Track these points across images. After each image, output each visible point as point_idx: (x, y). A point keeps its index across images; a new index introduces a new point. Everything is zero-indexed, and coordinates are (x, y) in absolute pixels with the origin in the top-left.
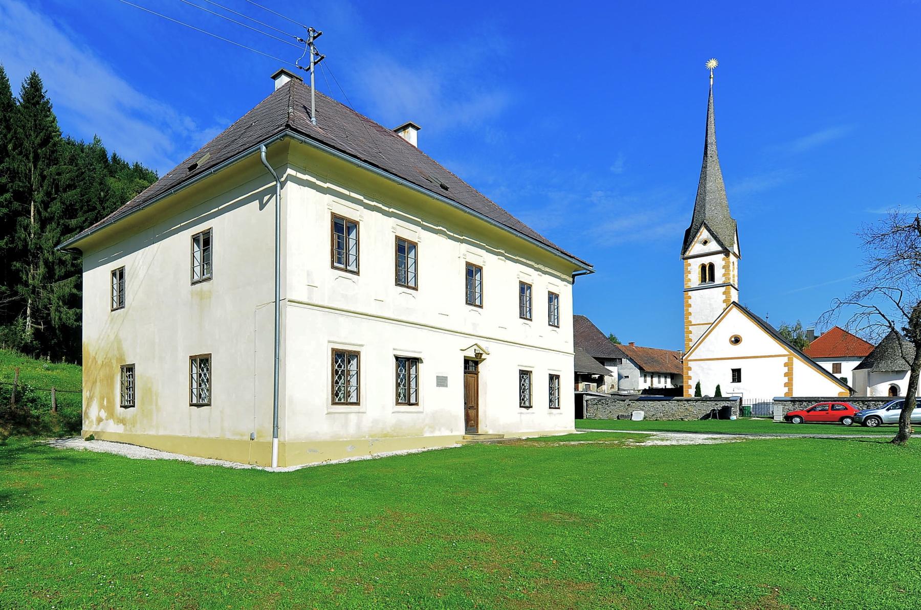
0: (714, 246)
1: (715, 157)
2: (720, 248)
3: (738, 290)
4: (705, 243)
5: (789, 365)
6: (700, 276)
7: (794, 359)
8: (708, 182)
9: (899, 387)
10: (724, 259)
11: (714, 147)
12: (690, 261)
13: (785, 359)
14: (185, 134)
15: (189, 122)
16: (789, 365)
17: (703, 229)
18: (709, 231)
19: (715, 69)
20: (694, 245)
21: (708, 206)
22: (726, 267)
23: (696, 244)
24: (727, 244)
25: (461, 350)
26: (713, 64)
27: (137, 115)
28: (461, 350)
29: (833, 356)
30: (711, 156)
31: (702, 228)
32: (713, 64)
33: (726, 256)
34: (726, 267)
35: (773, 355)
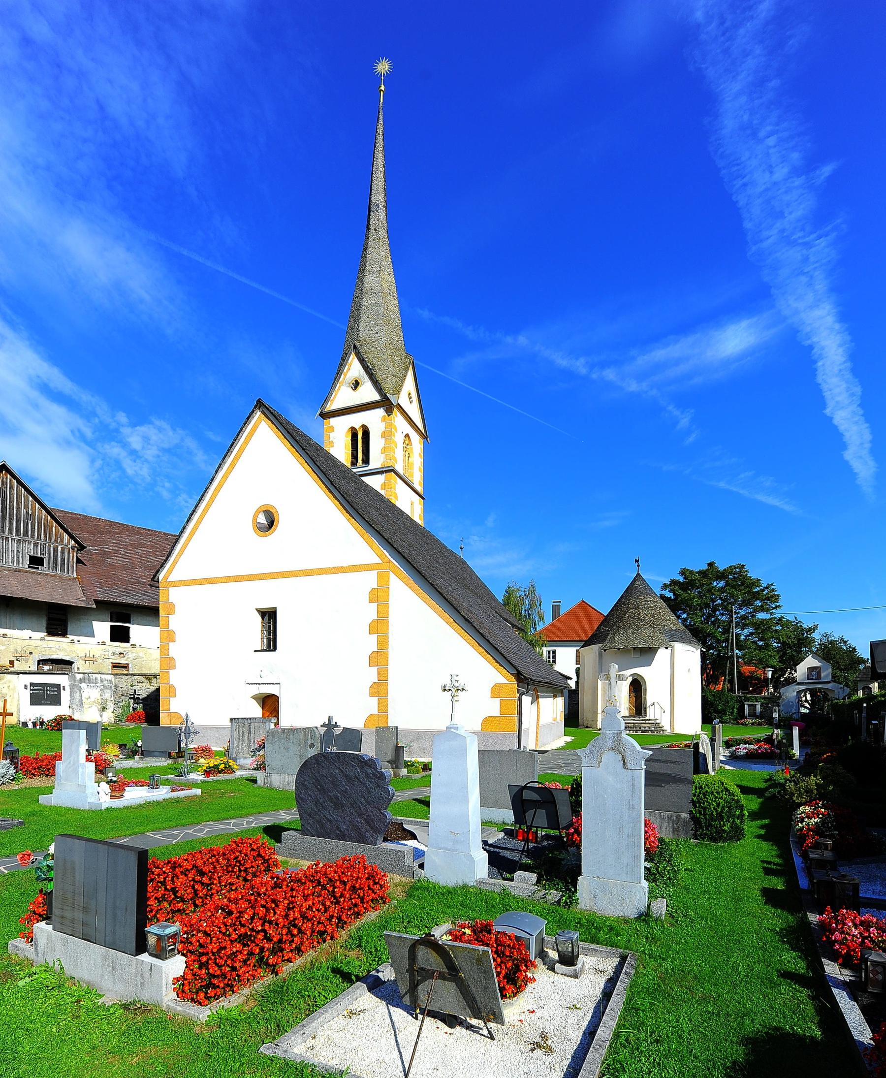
0: (368, 393)
1: (383, 233)
2: (376, 397)
3: (423, 498)
4: (356, 384)
5: (379, 597)
6: (350, 452)
7: (392, 577)
8: (367, 273)
9: (642, 677)
10: (383, 419)
11: (382, 215)
12: (333, 421)
13: (370, 580)
14: (113, 425)
15: (122, 417)
16: (379, 597)
17: (354, 358)
18: (362, 361)
19: (389, 77)
20: (339, 389)
21: (364, 317)
22: (387, 435)
23: (342, 387)
24: (388, 388)
25: (255, 651)
26: (383, 67)
27: (59, 398)
28: (255, 651)
29: (574, 639)
30: (375, 230)
31: (352, 357)
32: (383, 67)
33: (387, 412)
34: (387, 435)
35: (345, 565)
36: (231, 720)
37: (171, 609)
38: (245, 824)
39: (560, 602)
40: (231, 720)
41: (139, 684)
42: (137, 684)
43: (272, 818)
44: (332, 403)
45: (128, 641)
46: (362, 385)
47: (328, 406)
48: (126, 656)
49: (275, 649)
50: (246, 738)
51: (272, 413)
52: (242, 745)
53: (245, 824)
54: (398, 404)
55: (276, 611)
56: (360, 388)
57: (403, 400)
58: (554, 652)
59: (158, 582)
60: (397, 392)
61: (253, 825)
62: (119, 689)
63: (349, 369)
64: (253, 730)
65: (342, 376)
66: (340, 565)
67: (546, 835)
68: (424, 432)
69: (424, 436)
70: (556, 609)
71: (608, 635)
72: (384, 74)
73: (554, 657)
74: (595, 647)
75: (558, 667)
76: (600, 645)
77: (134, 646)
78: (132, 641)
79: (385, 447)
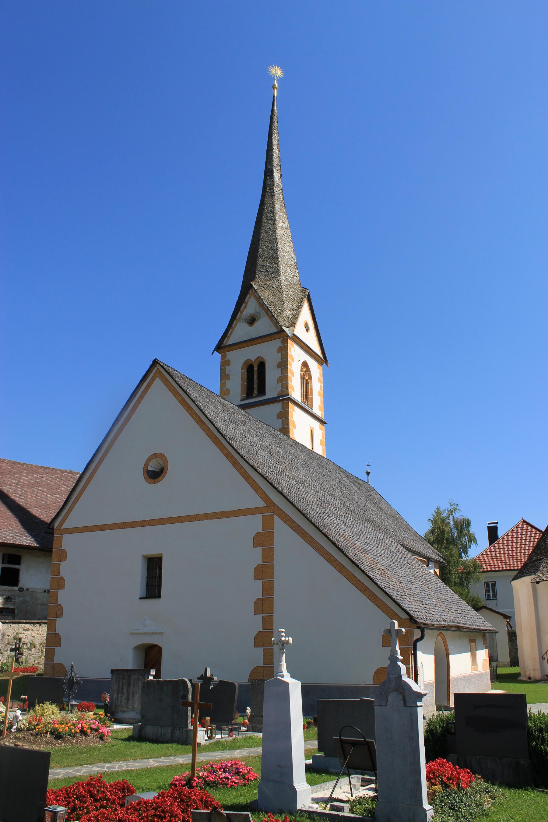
25: (212, 354)
28: (212, 354)
36: (113, 671)
37: (63, 556)
38: (117, 767)
39: (497, 523)
40: (113, 671)
41: (24, 632)
42: (23, 632)
43: (144, 764)
44: (228, 339)
45: (16, 585)
46: (258, 320)
47: (224, 342)
48: (13, 600)
49: (158, 596)
50: (125, 691)
51: (166, 371)
52: (121, 697)
53: (117, 767)
54: (294, 335)
55: (162, 557)
56: (256, 324)
57: (299, 331)
58: (494, 584)
59: (53, 529)
60: (293, 323)
61: (124, 769)
62: (6, 637)
63: (245, 307)
64: (132, 682)
65: (239, 313)
66: (225, 510)
67: (430, 803)
68: (322, 357)
69: (323, 360)
70: (493, 532)
71: (540, 565)
72: (277, 76)
73: (488, 591)
74: (527, 580)
75: (150, 677)
76: (532, 577)
77: (21, 589)
78: (20, 585)
79: (281, 377)
